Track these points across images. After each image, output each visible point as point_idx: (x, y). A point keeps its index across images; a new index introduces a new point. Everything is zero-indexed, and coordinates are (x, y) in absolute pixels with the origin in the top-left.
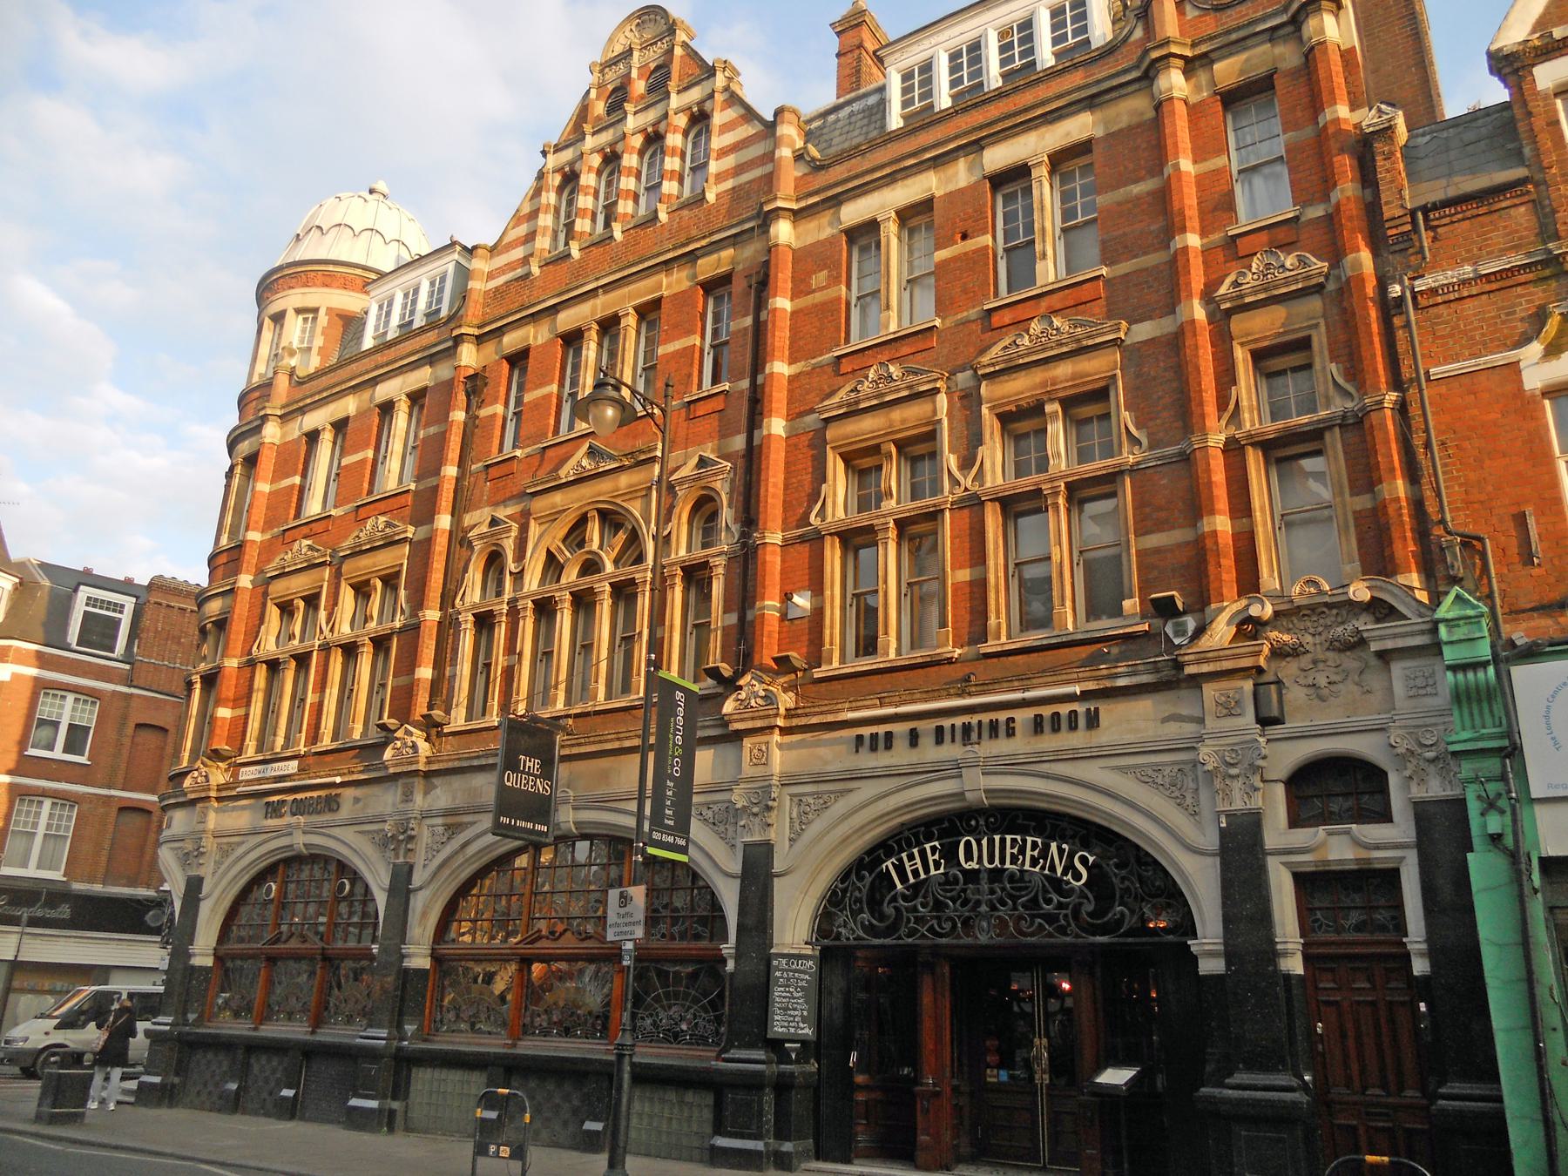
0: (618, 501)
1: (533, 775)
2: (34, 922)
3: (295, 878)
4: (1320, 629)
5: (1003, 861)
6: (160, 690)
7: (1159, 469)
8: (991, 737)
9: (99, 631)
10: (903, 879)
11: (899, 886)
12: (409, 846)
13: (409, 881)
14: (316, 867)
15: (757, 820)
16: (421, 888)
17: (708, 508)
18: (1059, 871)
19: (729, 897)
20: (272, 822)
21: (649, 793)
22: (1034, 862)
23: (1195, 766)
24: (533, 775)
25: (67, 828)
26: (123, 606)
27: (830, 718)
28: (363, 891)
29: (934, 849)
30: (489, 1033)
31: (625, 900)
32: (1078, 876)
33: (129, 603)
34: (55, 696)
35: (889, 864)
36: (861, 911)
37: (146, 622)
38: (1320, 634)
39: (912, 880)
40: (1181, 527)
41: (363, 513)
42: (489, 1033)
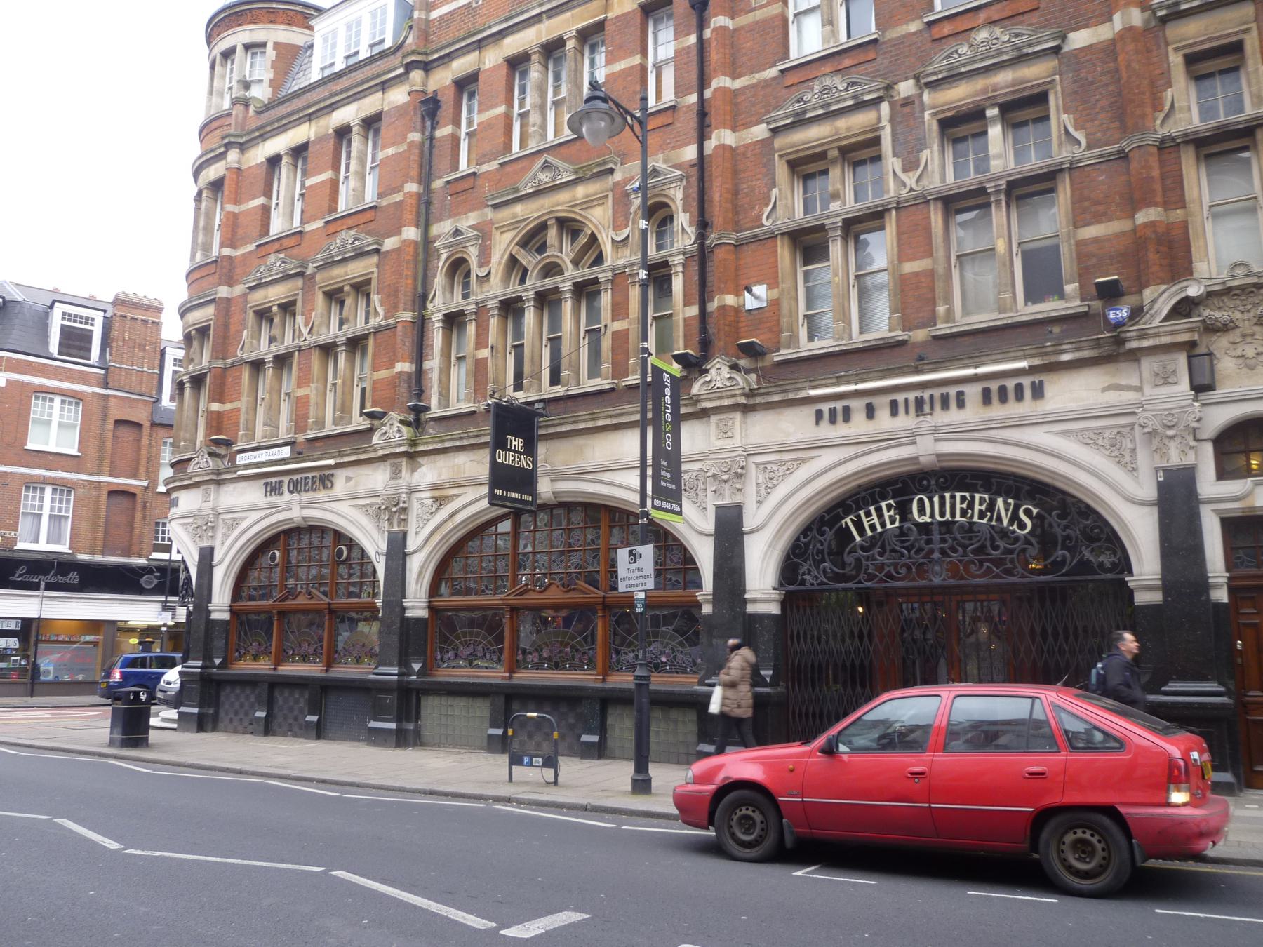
0: (577, 210)
1: (518, 452)
2: (50, 587)
3: (295, 546)
4: (1249, 307)
5: (953, 514)
6: (132, 391)
7: (1097, 167)
8: (943, 408)
9: (75, 341)
11: (858, 539)
12: (402, 517)
13: (404, 546)
14: (313, 535)
15: (727, 486)
16: (415, 552)
17: (462, 269)
18: (1005, 522)
19: (704, 554)
20: (274, 499)
21: (649, 462)
22: (982, 515)
23: (1132, 429)
24: (518, 452)
25: (67, 510)
26: (93, 319)
27: (791, 396)
28: (359, 556)
29: (889, 507)
30: (486, 668)
31: (634, 557)
32: (1022, 526)
33: (99, 318)
34: (44, 399)
35: (848, 521)
36: (823, 561)
37: (115, 333)
38: (1248, 311)
39: (869, 533)
40: (1118, 218)
41: (268, 248)
42: (486, 668)
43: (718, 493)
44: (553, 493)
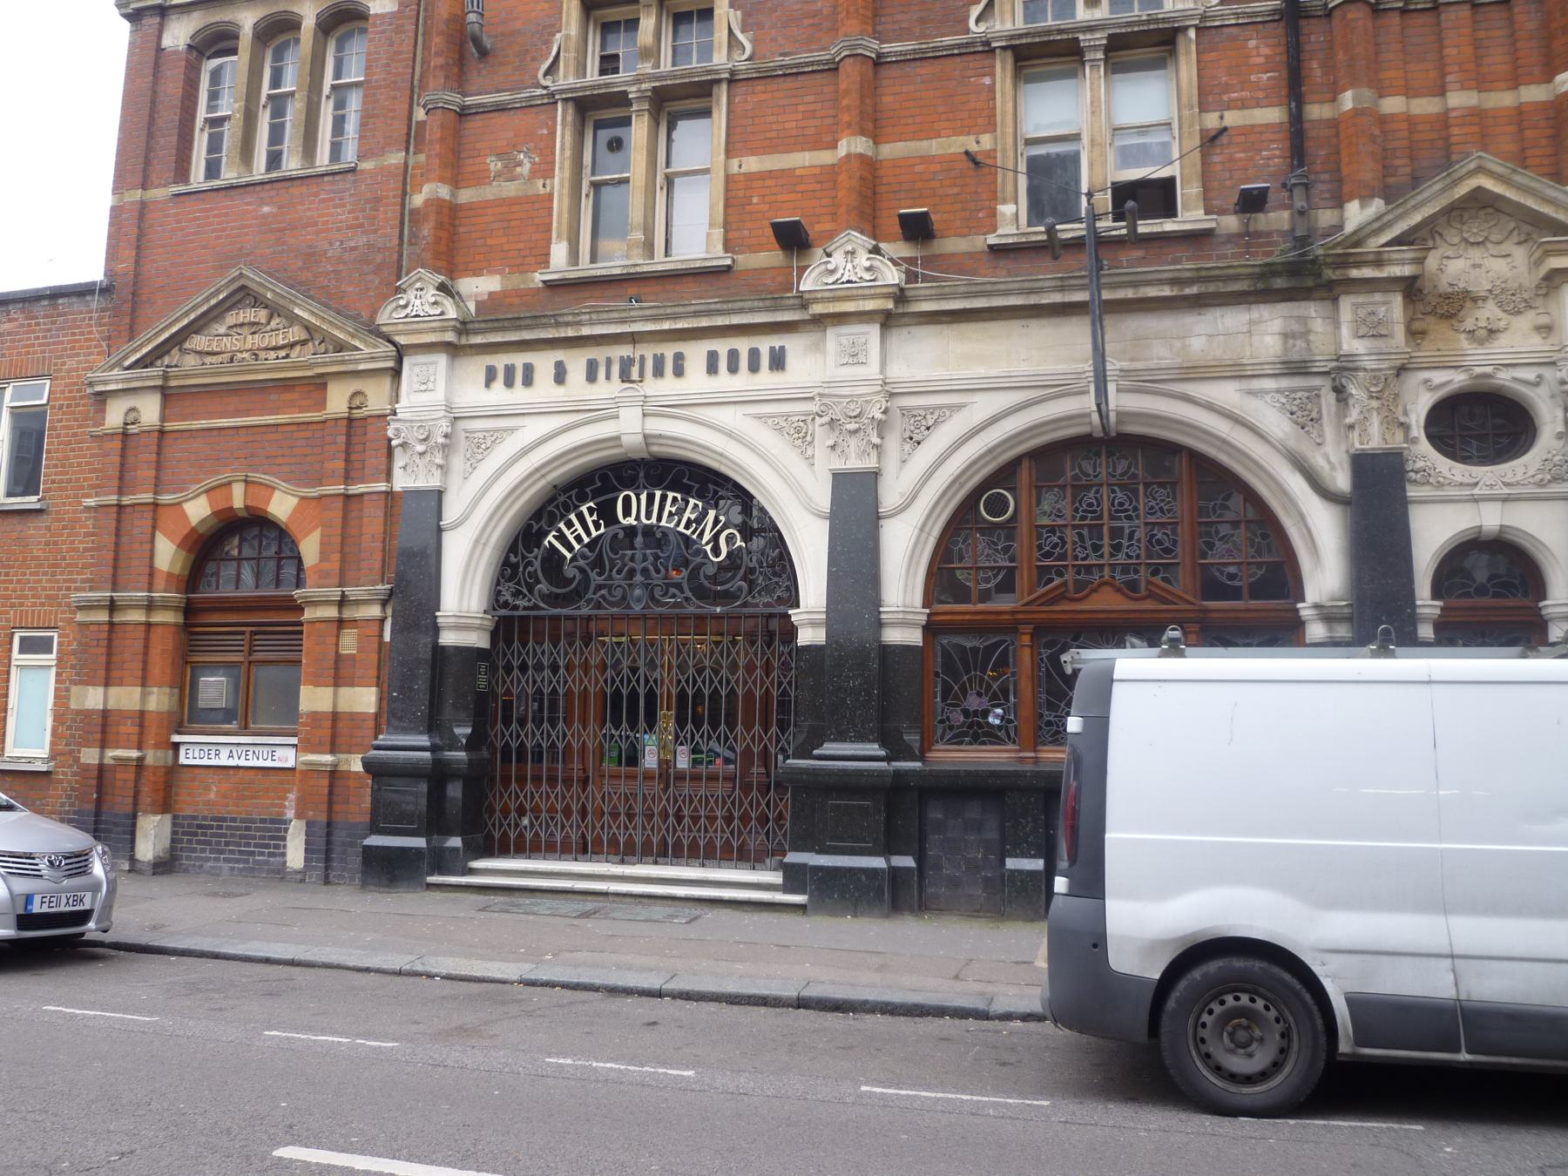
5: (659, 519)
10: (570, 548)
29: (591, 510)
43: (839, 450)
44: (646, 437)
